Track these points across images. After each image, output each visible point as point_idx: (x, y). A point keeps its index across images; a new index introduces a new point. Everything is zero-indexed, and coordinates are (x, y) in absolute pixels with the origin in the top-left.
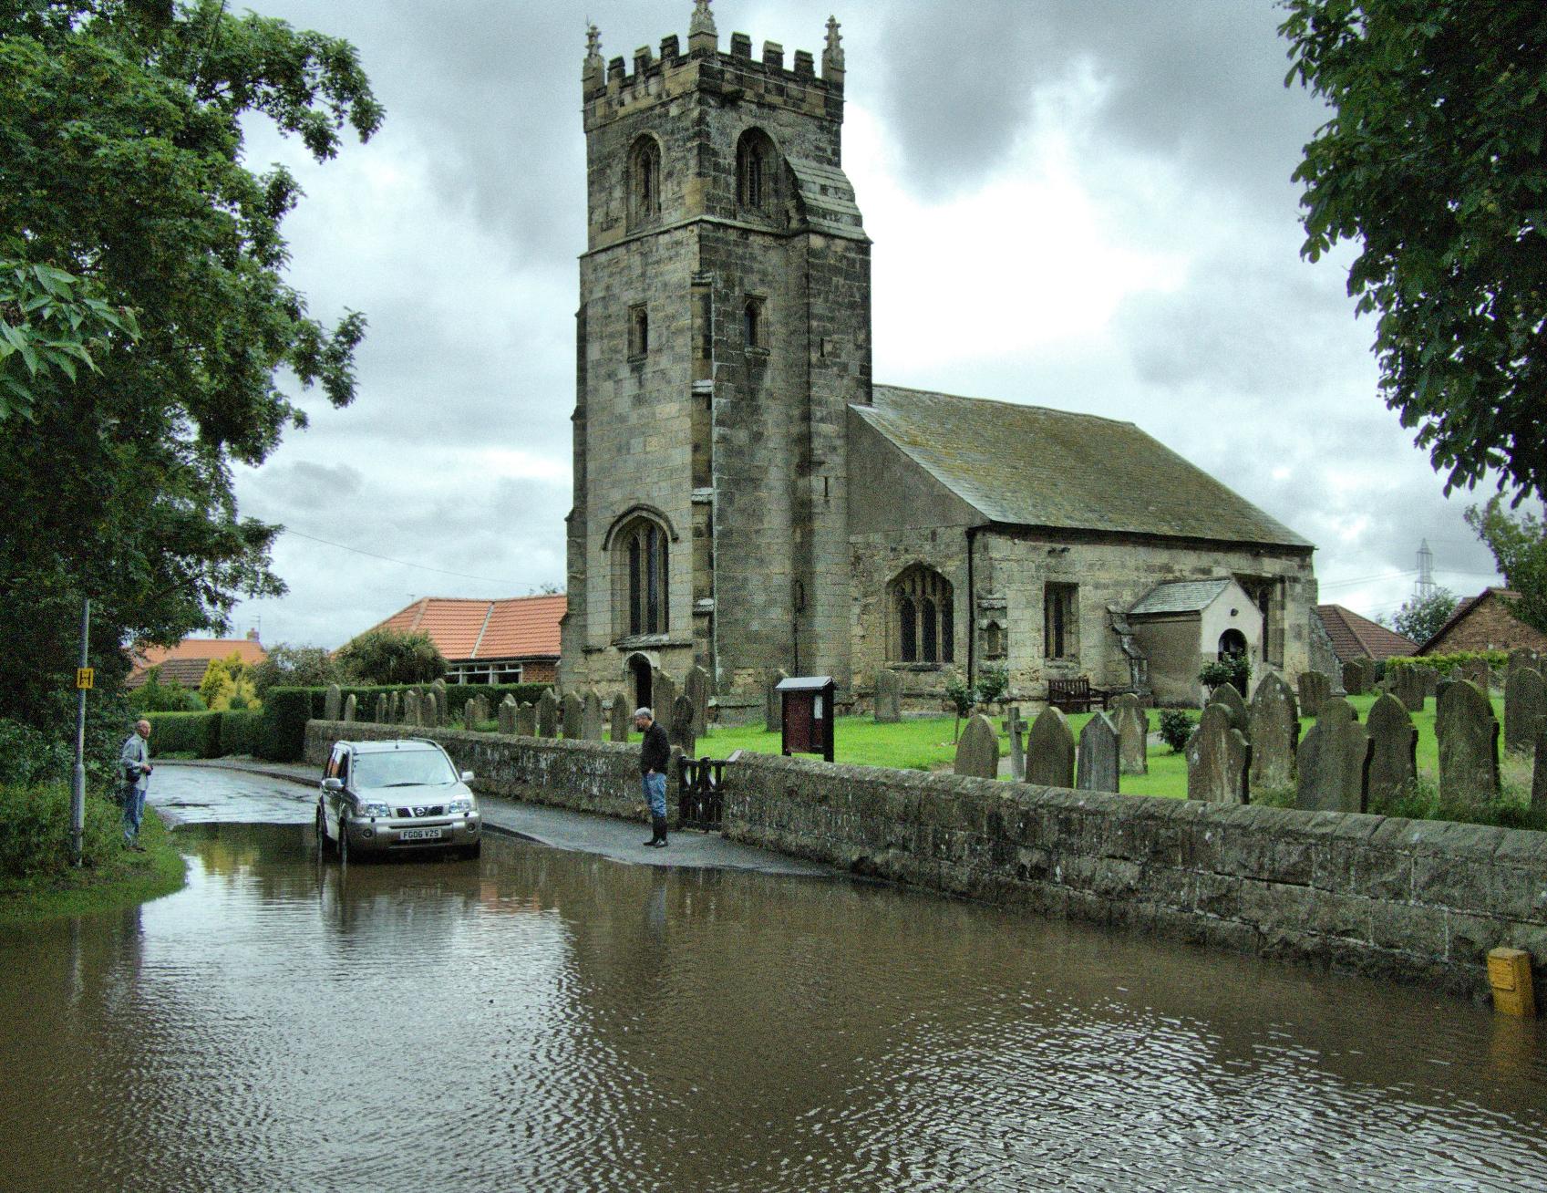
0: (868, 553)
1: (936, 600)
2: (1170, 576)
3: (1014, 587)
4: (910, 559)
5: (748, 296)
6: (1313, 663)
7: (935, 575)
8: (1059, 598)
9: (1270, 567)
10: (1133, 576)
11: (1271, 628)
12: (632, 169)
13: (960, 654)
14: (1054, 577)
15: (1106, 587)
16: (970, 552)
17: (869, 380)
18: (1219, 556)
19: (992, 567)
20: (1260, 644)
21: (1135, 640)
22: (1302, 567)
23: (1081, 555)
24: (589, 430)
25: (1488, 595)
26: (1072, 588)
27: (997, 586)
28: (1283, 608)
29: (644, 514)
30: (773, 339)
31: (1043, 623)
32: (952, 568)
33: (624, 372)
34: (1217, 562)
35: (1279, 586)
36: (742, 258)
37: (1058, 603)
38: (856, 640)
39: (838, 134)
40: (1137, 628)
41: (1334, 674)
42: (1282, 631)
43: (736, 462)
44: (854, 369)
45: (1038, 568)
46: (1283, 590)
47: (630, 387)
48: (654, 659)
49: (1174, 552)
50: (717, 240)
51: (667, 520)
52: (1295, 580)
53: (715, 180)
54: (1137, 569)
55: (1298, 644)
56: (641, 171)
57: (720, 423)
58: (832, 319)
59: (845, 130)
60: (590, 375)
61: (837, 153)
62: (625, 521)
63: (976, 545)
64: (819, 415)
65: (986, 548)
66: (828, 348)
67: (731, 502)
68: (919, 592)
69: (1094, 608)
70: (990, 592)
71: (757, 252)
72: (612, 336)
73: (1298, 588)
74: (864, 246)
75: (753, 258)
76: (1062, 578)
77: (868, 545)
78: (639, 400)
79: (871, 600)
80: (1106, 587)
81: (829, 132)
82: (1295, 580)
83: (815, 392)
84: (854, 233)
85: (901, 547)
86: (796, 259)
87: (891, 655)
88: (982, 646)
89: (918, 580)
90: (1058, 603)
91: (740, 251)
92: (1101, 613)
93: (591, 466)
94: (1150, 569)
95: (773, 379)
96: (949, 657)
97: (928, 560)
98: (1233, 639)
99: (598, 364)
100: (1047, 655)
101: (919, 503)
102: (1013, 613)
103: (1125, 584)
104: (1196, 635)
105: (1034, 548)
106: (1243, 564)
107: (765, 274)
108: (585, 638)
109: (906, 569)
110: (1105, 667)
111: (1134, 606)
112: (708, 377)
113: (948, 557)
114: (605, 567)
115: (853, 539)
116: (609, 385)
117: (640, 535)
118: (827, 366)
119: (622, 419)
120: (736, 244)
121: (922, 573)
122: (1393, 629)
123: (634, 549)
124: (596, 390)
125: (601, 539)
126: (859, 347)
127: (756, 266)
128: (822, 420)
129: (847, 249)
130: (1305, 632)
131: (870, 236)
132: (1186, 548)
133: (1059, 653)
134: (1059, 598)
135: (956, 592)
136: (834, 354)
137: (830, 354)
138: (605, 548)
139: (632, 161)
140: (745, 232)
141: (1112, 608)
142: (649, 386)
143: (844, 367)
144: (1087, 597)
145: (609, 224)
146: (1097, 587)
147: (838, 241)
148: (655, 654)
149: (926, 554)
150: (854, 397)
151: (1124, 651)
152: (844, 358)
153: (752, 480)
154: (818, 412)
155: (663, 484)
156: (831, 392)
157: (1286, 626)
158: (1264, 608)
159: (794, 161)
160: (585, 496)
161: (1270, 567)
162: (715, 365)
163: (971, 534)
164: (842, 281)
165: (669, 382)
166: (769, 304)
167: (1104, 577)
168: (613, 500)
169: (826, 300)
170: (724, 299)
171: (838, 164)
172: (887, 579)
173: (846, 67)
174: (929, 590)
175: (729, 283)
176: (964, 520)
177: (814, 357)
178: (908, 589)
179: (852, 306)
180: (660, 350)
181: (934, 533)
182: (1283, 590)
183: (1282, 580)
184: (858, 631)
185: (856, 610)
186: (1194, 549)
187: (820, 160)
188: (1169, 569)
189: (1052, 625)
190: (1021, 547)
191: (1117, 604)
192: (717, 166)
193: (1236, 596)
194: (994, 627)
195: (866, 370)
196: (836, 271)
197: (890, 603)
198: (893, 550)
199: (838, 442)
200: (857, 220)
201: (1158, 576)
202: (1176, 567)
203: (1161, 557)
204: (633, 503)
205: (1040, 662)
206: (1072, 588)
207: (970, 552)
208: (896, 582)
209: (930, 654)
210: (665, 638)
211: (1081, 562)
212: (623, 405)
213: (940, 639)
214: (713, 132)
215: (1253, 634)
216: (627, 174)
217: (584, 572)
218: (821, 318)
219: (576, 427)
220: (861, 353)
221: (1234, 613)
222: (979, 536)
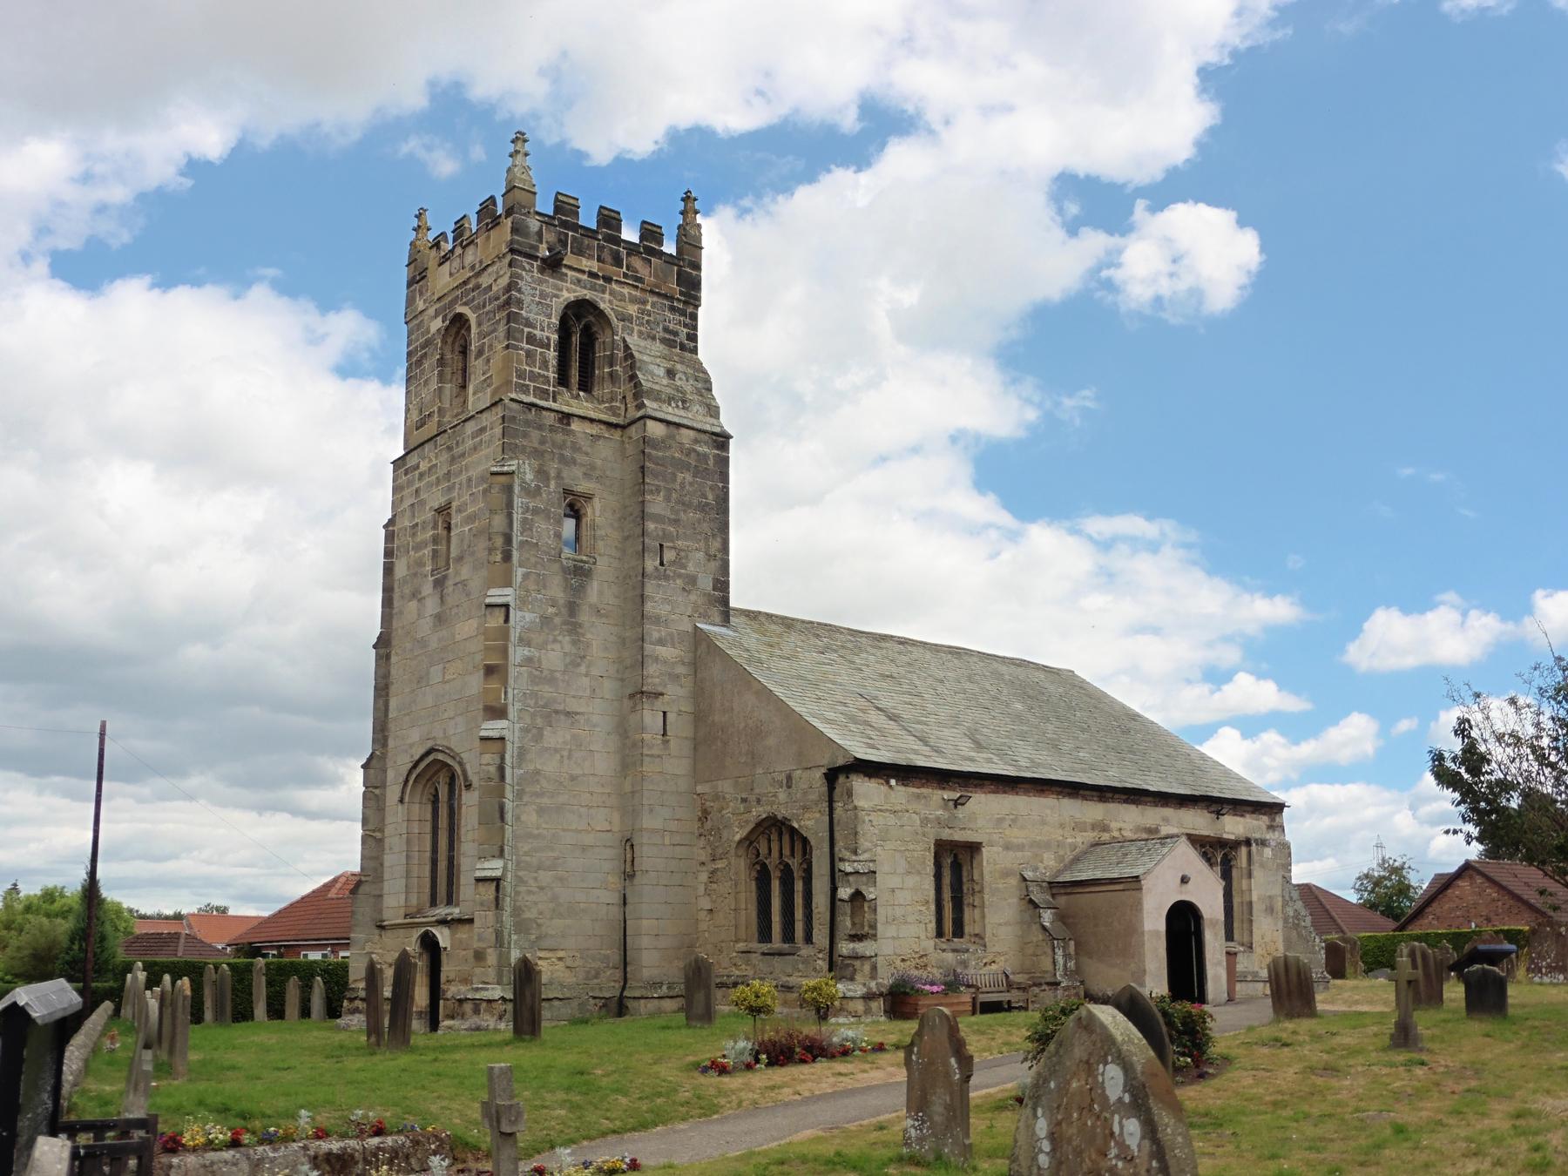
0: (716, 805)
1: (795, 863)
2: (1106, 837)
3: (889, 845)
4: (758, 812)
5: (567, 492)
6: (1288, 943)
7: (793, 832)
8: (955, 862)
9: (1233, 827)
10: (1057, 835)
11: (1236, 900)
12: (448, 356)
13: (821, 935)
14: (946, 834)
15: (1021, 847)
16: (831, 801)
17: (725, 601)
18: (1168, 812)
19: (856, 816)
20: (1220, 915)
21: (1062, 917)
22: (1271, 828)
23: (983, 804)
24: (394, 659)
25: (1467, 867)
26: (974, 848)
27: (864, 843)
28: (1250, 876)
29: (440, 757)
30: (600, 544)
31: (931, 894)
32: (811, 824)
33: (427, 589)
34: (1166, 820)
35: (1244, 850)
36: (562, 446)
37: (957, 868)
38: (703, 915)
39: (694, 317)
40: (1062, 901)
41: (1315, 958)
42: (1251, 903)
43: (546, 691)
44: (706, 583)
45: (925, 821)
46: (1249, 854)
47: (432, 606)
48: (443, 936)
49: (1111, 806)
50: (527, 423)
51: (461, 764)
52: (1263, 843)
53: (529, 354)
54: (1062, 826)
55: (1269, 920)
56: (458, 358)
57: (524, 642)
58: (676, 521)
59: (701, 312)
60: (396, 596)
61: (693, 338)
62: (422, 766)
63: (838, 791)
64: (656, 635)
65: (850, 794)
66: (669, 555)
67: (539, 737)
68: (775, 853)
69: (1006, 874)
70: (855, 853)
71: (585, 444)
72: (417, 548)
73: (1268, 852)
74: (721, 440)
75: (576, 448)
76: (959, 836)
77: (716, 797)
78: (440, 619)
79: (720, 865)
80: (1021, 847)
81: (683, 313)
82: (1263, 843)
83: (649, 607)
84: (695, 416)
85: (753, 798)
86: (630, 449)
87: (742, 933)
88: (846, 923)
89: (774, 837)
90: (957, 868)
91: (559, 437)
92: (1014, 881)
93: (393, 703)
94: (1079, 827)
95: (601, 593)
96: (808, 939)
97: (782, 813)
98: (1184, 920)
99: (404, 581)
100: (940, 933)
101: (771, 741)
102: (885, 880)
103: (1047, 846)
104: (1138, 906)
105: (918, 797)
106: (1198, 821)
107: (593, 467)
108: (380, 911)
109: (759, 825)
110: (1022, 950)
111: (1060, 872)
112: (508, 584)
113: (805, 808)
114: (406, 819)
115: (699, 789)
116: (413, 604)
117: (437, 777)
118: (667, 578)
119: (423, 643)
120: (552, 429)
121: (775, 827)
122: (1353, 897)
123: (435, 801)
124: (401, 613)
125: (397, 789)
126: (710, 557)
127: (579, 458)
128: (661, 642)
129: (696, 441)
130: (1279, 904)
131: (729, 429)
132: (1126, 801)
133: (959, 931)
134: (955, 862)
135: (815, 853)
136: (679, 563)
137: (673, 563)
138: (401, 801)
139: (448, 349)
140: (566, 417)
141: (1029, 875)
142: (450, 601)
143: (692, 580)
144: (992, 861)
145: (421, 424)
146: (1008, 847)
147: (684, 431)
148: (446, 931)
149: (782, 805)
150: (705, 616)
151: (1044, 928)
152: (691, 568)
153: (568, 714)
154: (654, 632)
155: (460, 719)
156: (671, 607)
157: (1255, 898)
158: (1227, 875)
159: (633, 341)
160: (385, 739)
161: (1233, 827)
162: (520, 572)
163: (832, 776)
164: (688, 477)
165: (468, 595)
166: (596, 502)
167: (1016, 835)
168: (408, 745)
169: (668, 499)
170: (533, 493)
171: (695, 351)
172: (737, 838)
173: (704, 243)
174: (786, 851)
175: (541, 473)
176: (826, 760)
177: (651, 564)
178: (763, 850)
179: (702, 508)
180: (460, 559)
181: (789, 778)
182: (1249, 854)
183: (1248, 842)
184: (705, 903)
185: (704, 877)
186: (1136, 802)
187: (670, 344)
188: (1105, 828)
189: (947, 895)
190: (899, 793)
191: (1035, 869)
192: (531, 339)
193: (1186, 857)
194: (858, 896)
195: (722, 585)
196: (683, 466)
197: (739, 868)
198: (744, 800)
199: (680, 670)
200: (714, 411)
201: (1091, 836)
202: (1114, 825)
203: (1093, 811)
204: (429, 744)
205: (929, 944)
206: (974, 848)
207: (831, 801)
208: (749, 841)
209: (788, 936)
210: (455, 912)
211: (983, 815)
212: (425, 625)
213: (799, 914)
214: (527, 299)
215: (1210, 902)
216: (441, 362)
217: (381, 830)
218: (658, 519)
219: (378, 658)
220: (714, 565)
221: (1184, 880)
222: (842, 779)
